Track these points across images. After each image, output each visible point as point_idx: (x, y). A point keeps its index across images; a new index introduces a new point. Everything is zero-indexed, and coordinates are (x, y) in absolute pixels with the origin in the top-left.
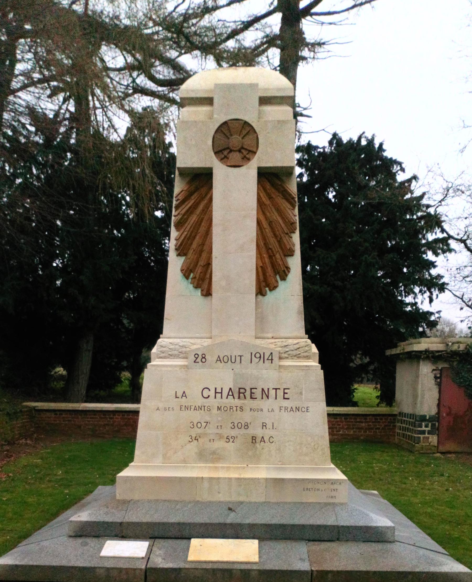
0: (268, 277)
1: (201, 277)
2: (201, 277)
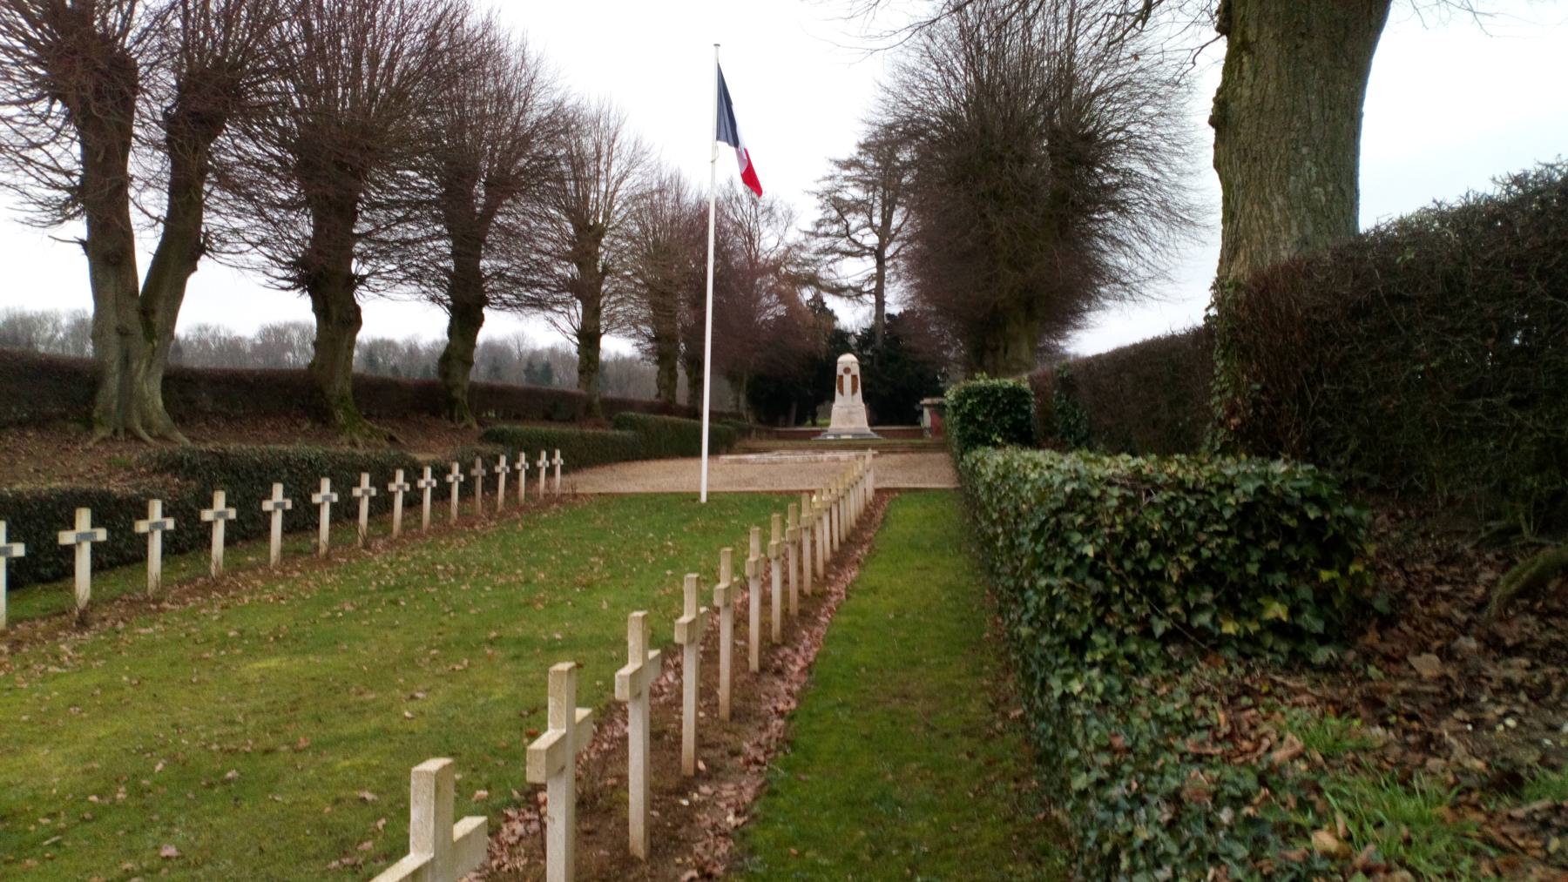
0: (854, 391)
1: (842, 392)
2: (842, 392)
